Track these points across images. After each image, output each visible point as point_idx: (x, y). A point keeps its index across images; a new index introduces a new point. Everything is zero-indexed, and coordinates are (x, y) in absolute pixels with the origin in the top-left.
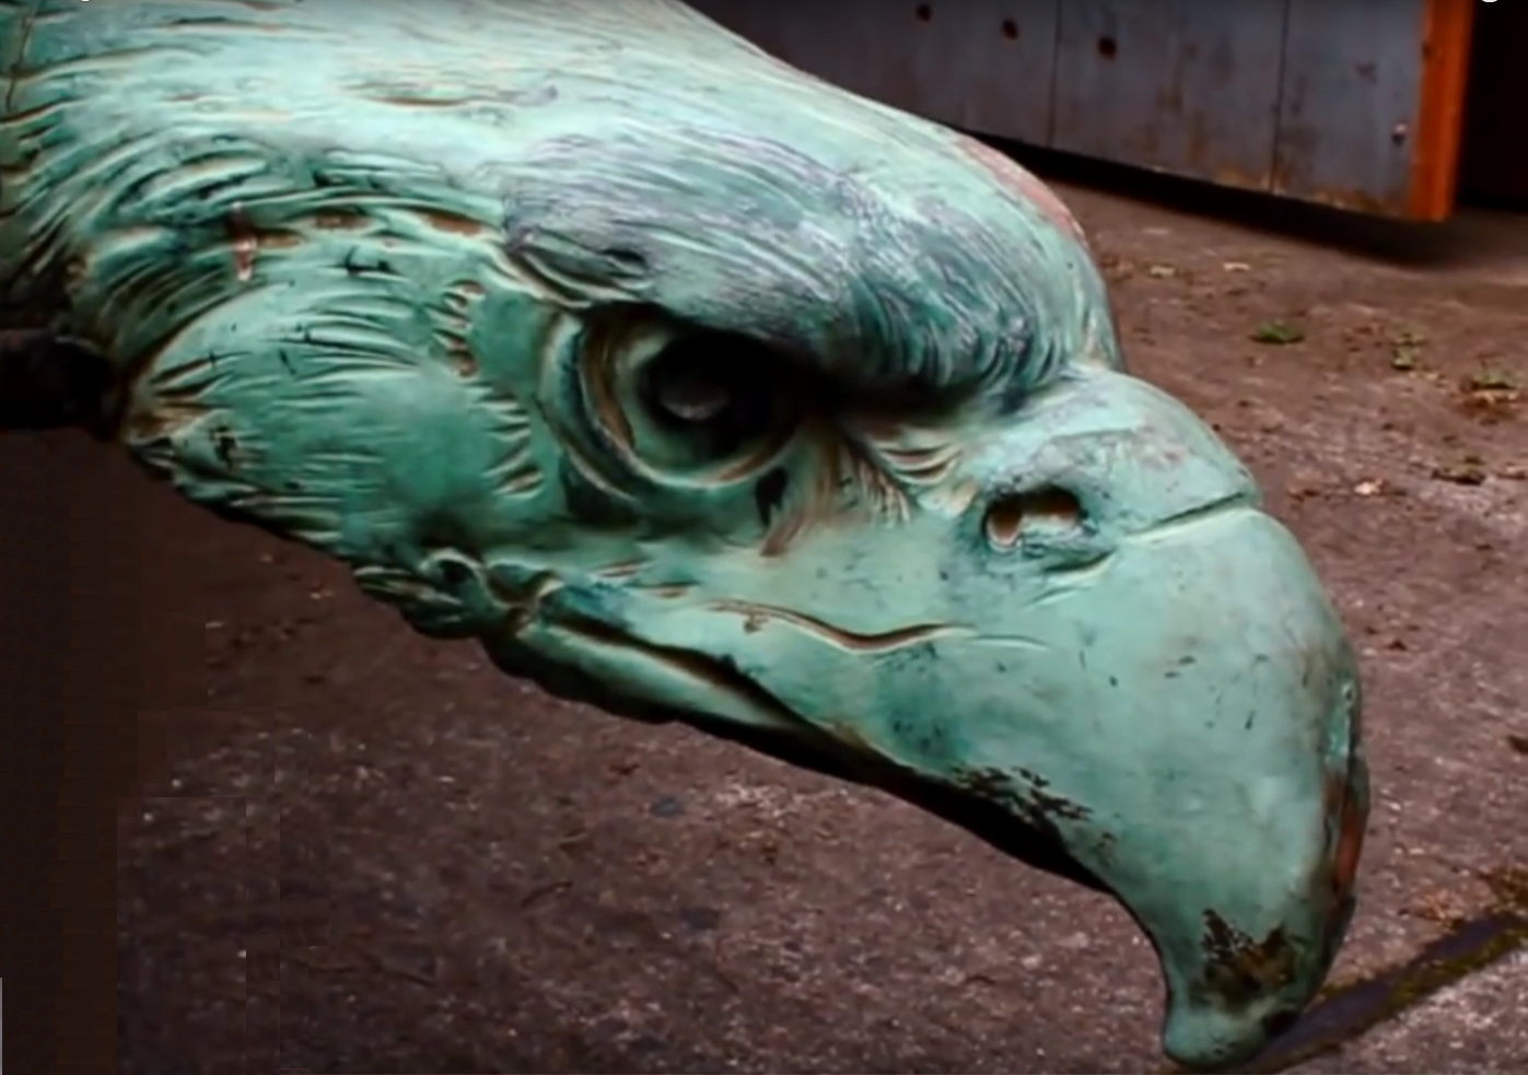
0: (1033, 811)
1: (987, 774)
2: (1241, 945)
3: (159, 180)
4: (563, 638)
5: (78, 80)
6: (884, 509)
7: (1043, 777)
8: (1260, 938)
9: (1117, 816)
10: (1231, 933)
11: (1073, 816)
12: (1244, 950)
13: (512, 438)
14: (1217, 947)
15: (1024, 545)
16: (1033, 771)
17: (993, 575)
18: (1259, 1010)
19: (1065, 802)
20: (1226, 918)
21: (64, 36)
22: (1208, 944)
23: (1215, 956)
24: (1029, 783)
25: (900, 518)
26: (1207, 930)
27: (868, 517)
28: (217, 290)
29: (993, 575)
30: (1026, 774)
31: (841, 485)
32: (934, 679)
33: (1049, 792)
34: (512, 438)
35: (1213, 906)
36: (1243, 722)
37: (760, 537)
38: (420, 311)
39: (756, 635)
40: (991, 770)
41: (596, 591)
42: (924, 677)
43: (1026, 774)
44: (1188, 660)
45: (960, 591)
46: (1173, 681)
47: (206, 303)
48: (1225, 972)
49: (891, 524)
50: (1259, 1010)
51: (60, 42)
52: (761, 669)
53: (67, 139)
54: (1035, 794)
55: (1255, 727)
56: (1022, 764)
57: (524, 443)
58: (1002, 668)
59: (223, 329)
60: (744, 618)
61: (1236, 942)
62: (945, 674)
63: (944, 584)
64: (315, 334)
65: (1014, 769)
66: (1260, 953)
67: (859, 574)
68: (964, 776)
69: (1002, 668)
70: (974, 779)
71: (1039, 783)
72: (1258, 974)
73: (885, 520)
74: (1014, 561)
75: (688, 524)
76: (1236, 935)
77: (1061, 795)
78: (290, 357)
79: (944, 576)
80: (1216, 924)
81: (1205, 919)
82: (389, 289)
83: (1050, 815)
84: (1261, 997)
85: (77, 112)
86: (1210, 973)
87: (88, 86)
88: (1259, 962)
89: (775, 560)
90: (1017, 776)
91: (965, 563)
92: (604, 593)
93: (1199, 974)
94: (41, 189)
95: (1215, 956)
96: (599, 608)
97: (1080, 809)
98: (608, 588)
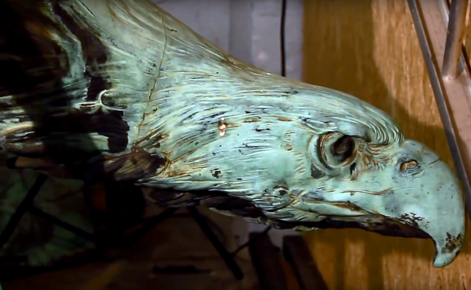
0: (413, 221)
1: (404, 215)
2: (453, 238)
3: (225, 113)
4: (307, 204)
5: (170, 92)
6: (379, 168)
7: (415, 213)
8: (456, 236)
9: (430, 218)
10: (451, 236)
11: (421, 220)
12: (454, 239)
13: (300, 162)
14: (449, 240)
15: (408, 171)
16: (413, 212)
17: (403, 177)
18: (455, 251)
19: (420, 217)
20: (450, 233)
21: (166, 82)
22: (447, 239)
23: (448, 242)
24: (412, 215)
25: (382, 169)
26: (447, 237)
27: (375, 170)
28: (214, 138)
29: (403, 177)
30: (412, 213)
31: (367, 165)
32: (394, 198)
33: (415, 216)
34: (300, 162)
35: (448, 232)
36: (451, 197)
37: (350, 177)
38: (279, 138)
39: (353, 196)
40: (405, 214)
41: (316, 192)
42: (392, 198)
43: (412, 213)
44: (441, 187)
45: (397, 181)
46: (438, 191)
47: (211, 140)
48: (450, 244)
49: (381, 170)
50: (455, 251)
51: (164, 84)
52: (357, 202)
53: (169, 106)
54: (413, 217)
55: (453, 197)
56: (411, 212)
57: (303, 163)
58: (407, 194)
59: (216, 146)
60: (350, 193)
61: (452, 238)
62: (396, 196)
63: (393, 180)
64: (249, 145)
65: (409, 213)
66: (456, 239)
67: (376, 180)
68: (400, 216)
69: (407, 194)
70: (402, 216)
71: (414, 215)
72: (456, 244)
73: (379, 170)
74: (407, 174)
75: (336, 176)
76: (452, 236)
77: (419, 216)
78: (242, 151)
79: (393, 178)
80: (449, 235)
81: (446, 235)
82: (269, 134)
83: (416, 221)
84: (456, 248)
85: (170, 100)
86: (447, 245)
87: (173, 93)
88: (456, 241)
89: (355, 181)
90: (410, 214)
91: (397, 175)
92: (318, 193)
93: (444, 246)
94: (158, 118)
95: (448, 242)
96: (317, 196)
97: (422, 218)
98: (318, 191)
